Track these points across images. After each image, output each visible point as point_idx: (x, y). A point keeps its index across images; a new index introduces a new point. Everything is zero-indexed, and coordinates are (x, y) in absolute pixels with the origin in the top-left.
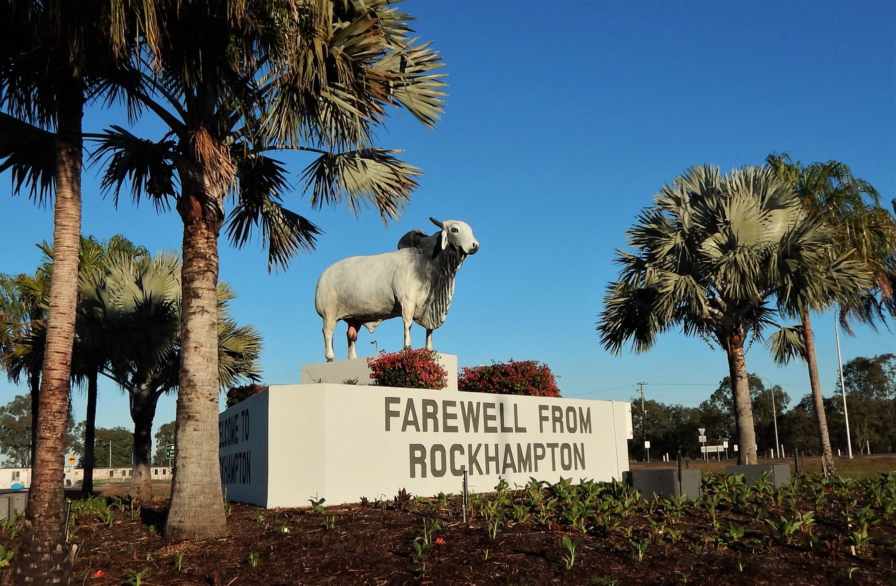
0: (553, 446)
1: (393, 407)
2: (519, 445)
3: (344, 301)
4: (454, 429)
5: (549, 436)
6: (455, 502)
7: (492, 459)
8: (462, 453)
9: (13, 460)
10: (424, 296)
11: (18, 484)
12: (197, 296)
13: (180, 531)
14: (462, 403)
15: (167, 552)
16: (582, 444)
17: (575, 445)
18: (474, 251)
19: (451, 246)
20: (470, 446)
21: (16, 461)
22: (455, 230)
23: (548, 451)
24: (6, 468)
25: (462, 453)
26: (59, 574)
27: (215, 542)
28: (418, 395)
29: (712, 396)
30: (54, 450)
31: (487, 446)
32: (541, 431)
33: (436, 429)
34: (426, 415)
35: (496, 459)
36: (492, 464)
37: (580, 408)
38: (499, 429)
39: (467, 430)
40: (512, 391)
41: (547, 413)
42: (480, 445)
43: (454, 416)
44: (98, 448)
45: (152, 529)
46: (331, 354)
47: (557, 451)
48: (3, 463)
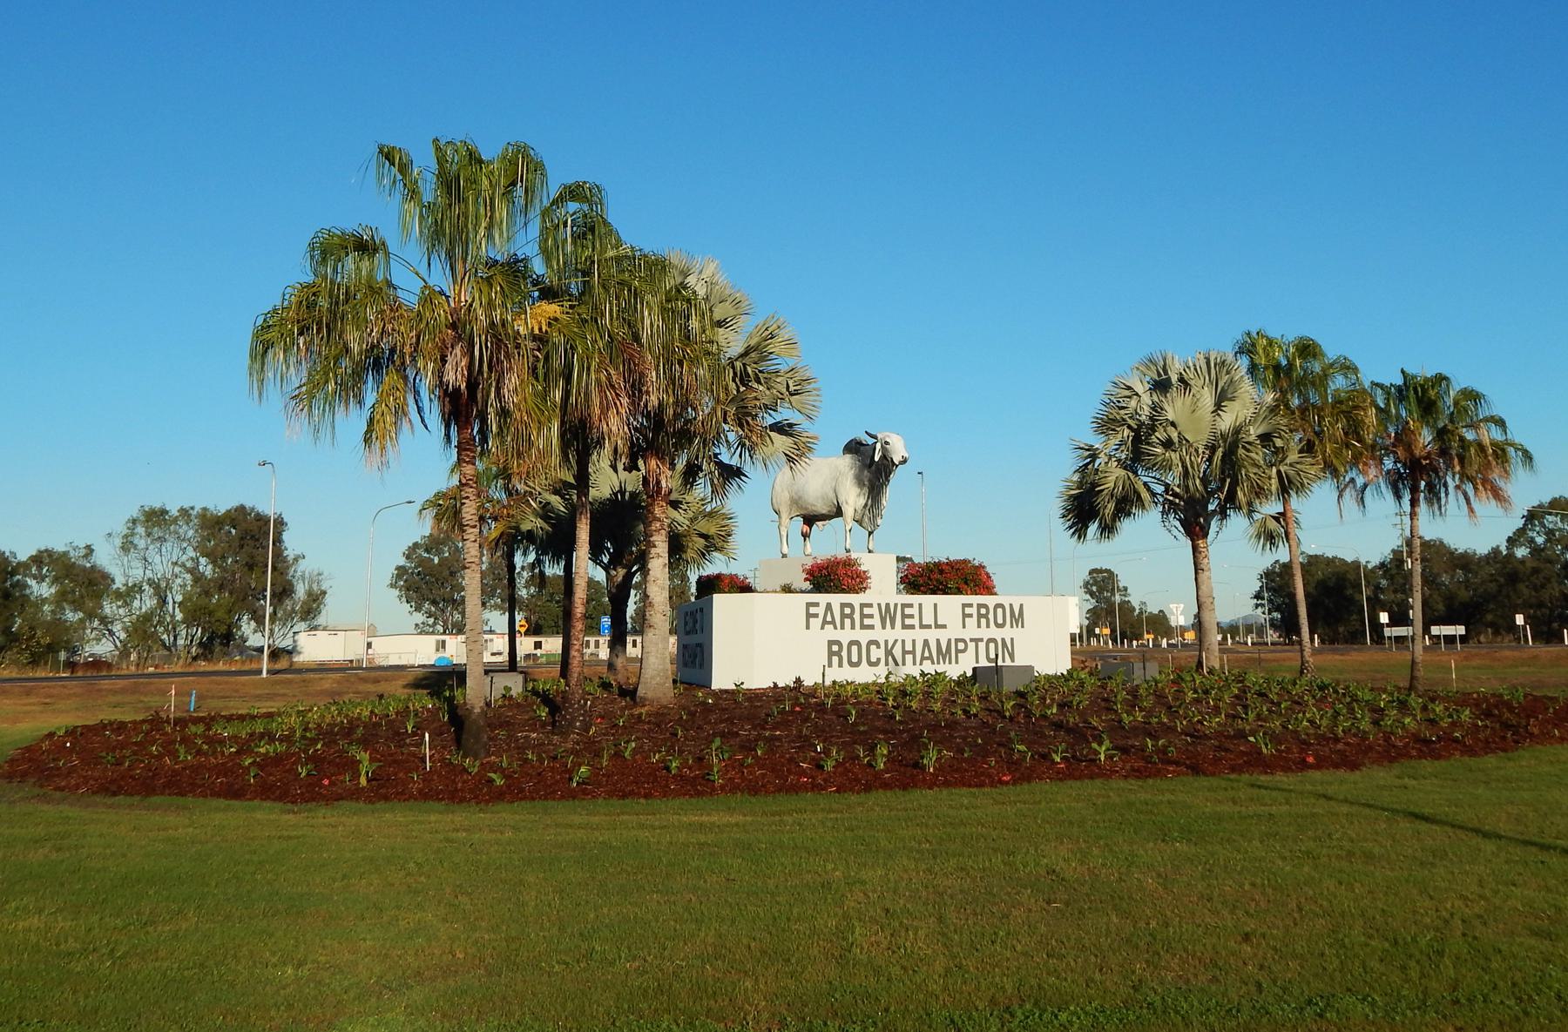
0: (977, 641)
1: (813, 610)
2: (938, 640)
3: (796, 502)
4: (871, 627)
5: (972, 630)
6: (879, 690)
7: (909, 652)
8: (878, 647)
9: (431, 621)
10: (862, 501)
11: (444, 658)
12: (655, 546)
13: (645, 699)
14: (879, 605)
15: (636, 711)
16: (1012, 639)
17: (1003, 640)
18: (904, 461)
19: (884, 457)
20: (886, 642)
21: (435, 623)
22: (887, 443)
23: (972, 646)
24: (420, 633)
25: (878, 647)
26: (583, 715)
27: (666, 707)
28: (836, 599)
29: (1509, 540)
30: (578, 650)
31: (903, 641)
32: (964, 627)
33: (853, 627)
34: (843, 616)
35: (913, 652)
36: (909, 658)
37: (1011, 605)
38: (917, 626)
39: (884, 627)
40: (945, 591)
41: (973, 611)
42: (896, 641)
43: (871, 616)
44: (549, 604)
45: (628, 698)
46: (785, 550)
47: (982, 646)
48: (417, 625)
